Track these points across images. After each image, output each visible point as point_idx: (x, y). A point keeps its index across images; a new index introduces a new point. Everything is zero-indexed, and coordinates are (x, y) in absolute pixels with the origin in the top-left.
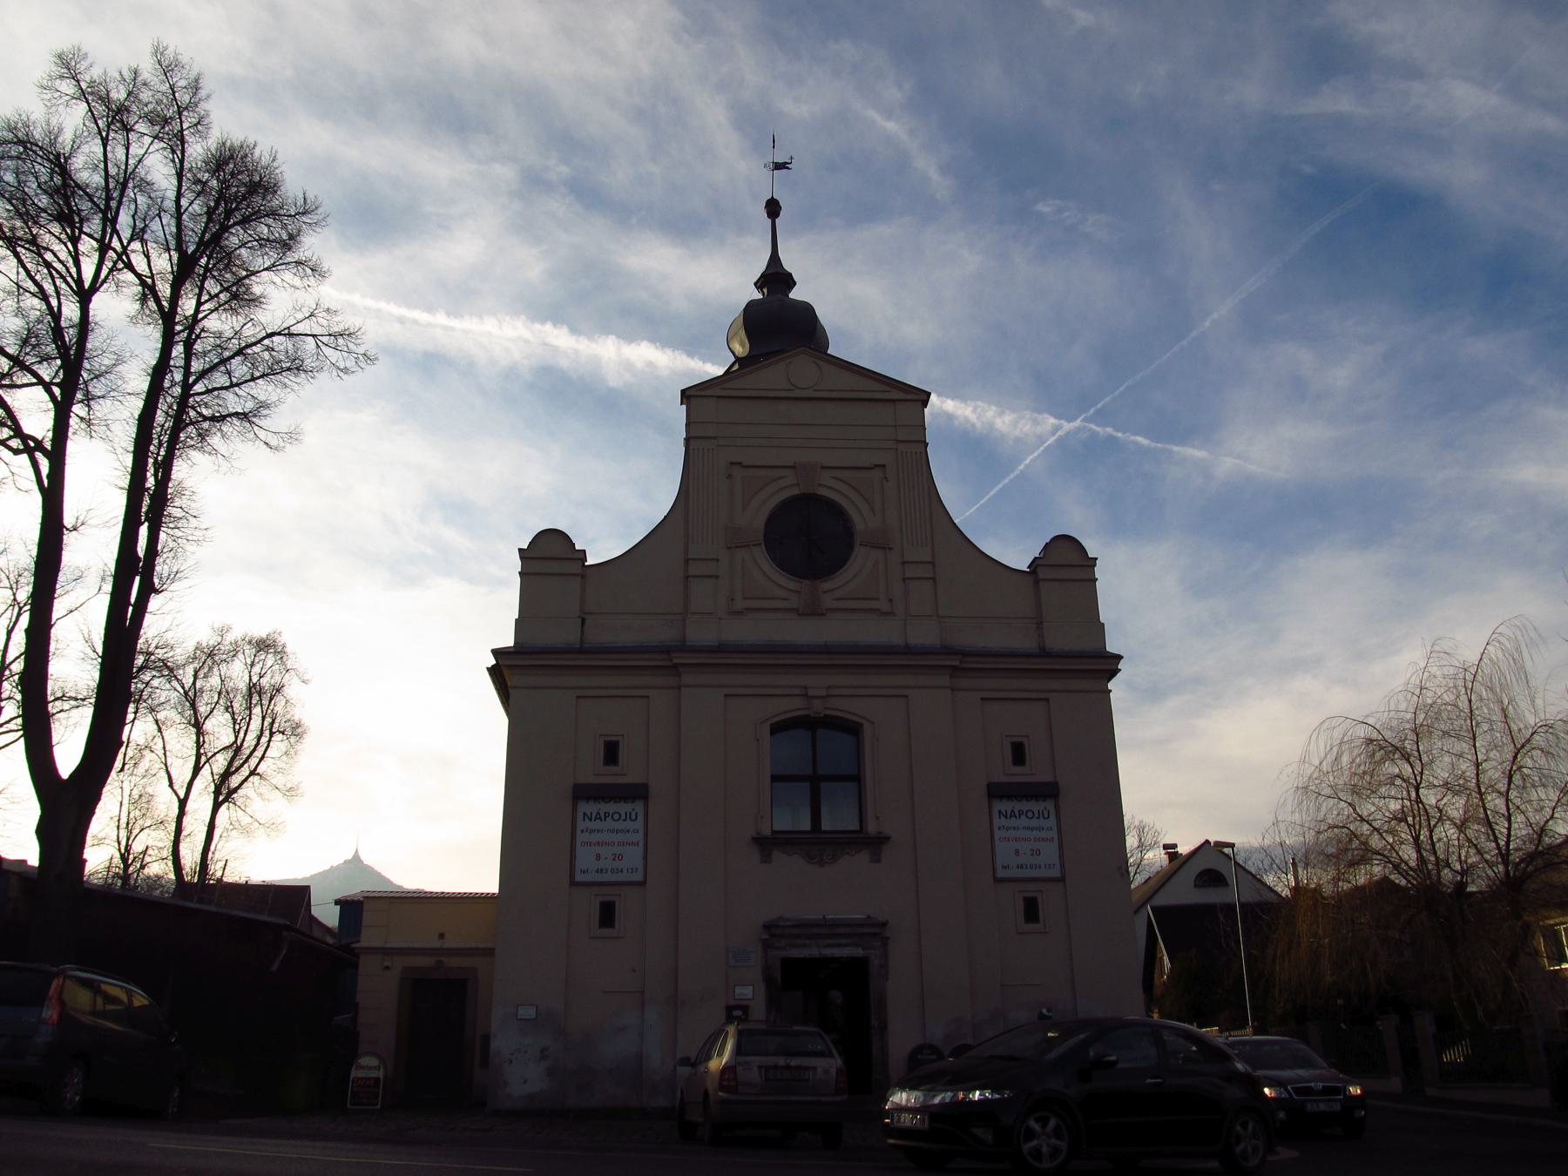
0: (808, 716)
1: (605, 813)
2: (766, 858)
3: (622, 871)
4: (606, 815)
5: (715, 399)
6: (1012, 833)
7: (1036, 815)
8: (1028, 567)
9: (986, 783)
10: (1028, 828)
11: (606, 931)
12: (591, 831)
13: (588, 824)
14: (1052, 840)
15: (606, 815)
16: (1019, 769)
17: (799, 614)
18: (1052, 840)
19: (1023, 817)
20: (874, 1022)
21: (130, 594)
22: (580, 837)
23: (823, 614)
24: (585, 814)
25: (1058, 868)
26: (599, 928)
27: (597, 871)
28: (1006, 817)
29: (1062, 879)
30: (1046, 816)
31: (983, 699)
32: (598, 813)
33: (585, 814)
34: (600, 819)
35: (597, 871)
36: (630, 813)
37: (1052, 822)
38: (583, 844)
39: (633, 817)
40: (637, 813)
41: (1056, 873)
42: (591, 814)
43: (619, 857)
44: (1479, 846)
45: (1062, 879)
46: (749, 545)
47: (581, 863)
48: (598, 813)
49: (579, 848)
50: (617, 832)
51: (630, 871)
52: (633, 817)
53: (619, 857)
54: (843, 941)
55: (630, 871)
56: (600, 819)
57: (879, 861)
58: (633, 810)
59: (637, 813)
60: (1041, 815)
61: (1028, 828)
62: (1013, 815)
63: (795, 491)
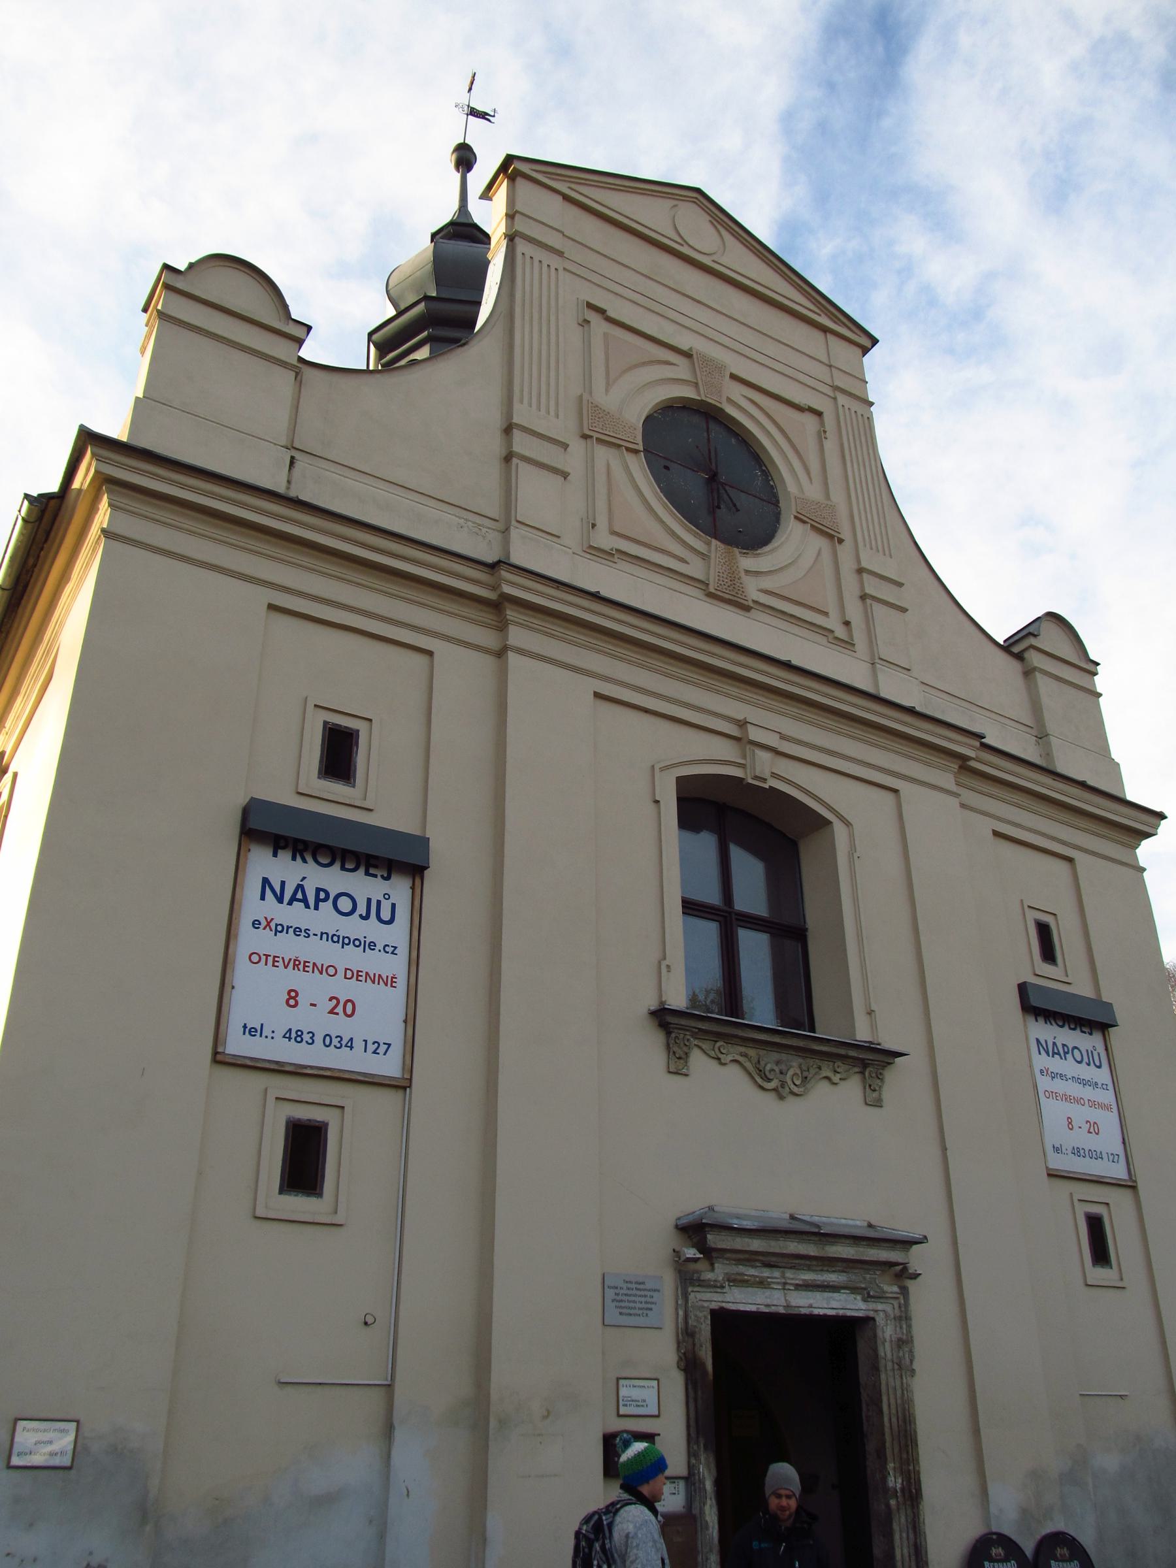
0: (740, 780)
1: (318, 890)
2: (677, 1064)
3: (350, 1045)
4: (322, 896)
5: (560, 198)
6: (287, 946)
7: (361, 909)
8: (1005, 641)
9: (242, 801)
10: (334, 938)
11: (299, 1205)
12: (280, 929)
13: (271, 908)
14: (391, 982)
15: (322, 896)
16: (336, 789)
17: (710, 595)
18: (391, 982)
19: (326, 907)
20: (894, 1481)
21: (156, 334)
22: (249, 940)
23: (747, 609)
24: (266, 881)
25: (396, 1052)
26: (281, 1192)
27: (288, 1035)
28: (280, 900)
29: (402, 1086)
30: (386, 916)
31: (271, 607)
32: (300, 887)
33: (266, 881)
34: (305, 901)
35: (288, 1035)
36: (379, 902)
37: (398, 934)
38: (255, 958)
39: (386, 915)
40: (393, 906)
41: (389, 1066)
42: (283, 883)
43: (345, 1007)
44: (712, 1048)
45: (402, 1086)
46: (619, 446)
47: (240, 1012)
48: (300, 887)
49: (243, 970)
50: (345, 942)
51: (371, 1048)
52: (386, 915)
53: (345, 1007)
54: (832, 1278)
55: (371, 1048)
56: (305, 901)
57: (878, 1104)
58: (387, 896)
59: (393, 906)
60: (372, 911)
61: (334, 938)
62: (299, 896)
63: (688, 393)
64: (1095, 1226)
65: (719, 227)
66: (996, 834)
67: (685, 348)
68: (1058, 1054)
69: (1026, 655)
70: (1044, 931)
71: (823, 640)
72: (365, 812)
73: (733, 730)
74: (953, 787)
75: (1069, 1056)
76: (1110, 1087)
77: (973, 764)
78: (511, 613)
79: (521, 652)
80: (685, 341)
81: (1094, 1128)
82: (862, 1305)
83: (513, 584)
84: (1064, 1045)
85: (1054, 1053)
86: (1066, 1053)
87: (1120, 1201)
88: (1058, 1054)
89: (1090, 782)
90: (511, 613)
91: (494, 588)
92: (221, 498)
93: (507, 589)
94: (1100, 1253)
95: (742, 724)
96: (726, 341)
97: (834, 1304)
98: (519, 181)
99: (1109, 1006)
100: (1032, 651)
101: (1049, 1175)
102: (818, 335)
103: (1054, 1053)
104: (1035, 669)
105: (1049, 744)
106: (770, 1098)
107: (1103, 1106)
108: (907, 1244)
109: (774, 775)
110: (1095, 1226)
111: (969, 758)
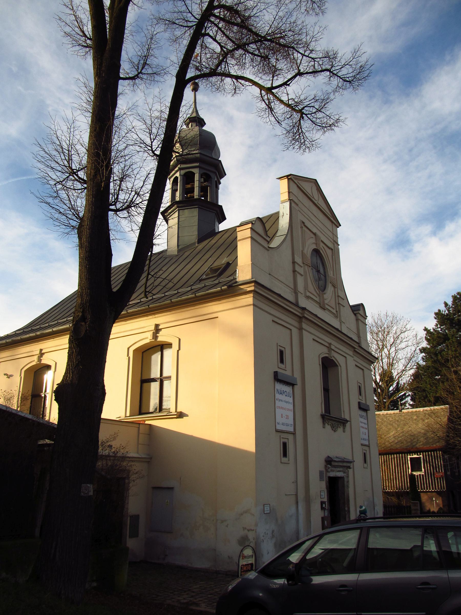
17: (321, 307)
23: (324, 309)
64: (285, 445)
65: (319, 194)
66: (356, 365)
67: (314, 232)
68: (281, 393)
69: (357, 315)
70: (281, 353)
71: (333, 316)
72: (285, 371)
73: (327, 345)
74: (352, 355)
75: (284, 394)
76: (292, 404)
77: (356, 350)
78: (304, 320)
79: (305, 330)
80: (314, 230)
81: (287, 417)
82: (343, 474)
83: (307, 314)
84: (283, 391)
85: (281, 393)
86: (283, 393)
87: (291, 437)
88: (281, 393)
89: (282, 295)
90: (304, 320)
91: (302, 314)
92: (280, 301)
93: (306, 315)
94: (285, 454)
95: (330, 344)
96: (319, 228)
97: (333, 474)
98: (290, 180)
99: (368, 406)
100: (359, 314)
101: (276, 431)
102: (330, 223)
103: (281, 393)
104: (359, 319)
105: (360, 339)
106: (333, 431)
107: (288, 410)
108: (350, 462)
109: (333, 357)
110: (285, 445)
111: (356, 348)
